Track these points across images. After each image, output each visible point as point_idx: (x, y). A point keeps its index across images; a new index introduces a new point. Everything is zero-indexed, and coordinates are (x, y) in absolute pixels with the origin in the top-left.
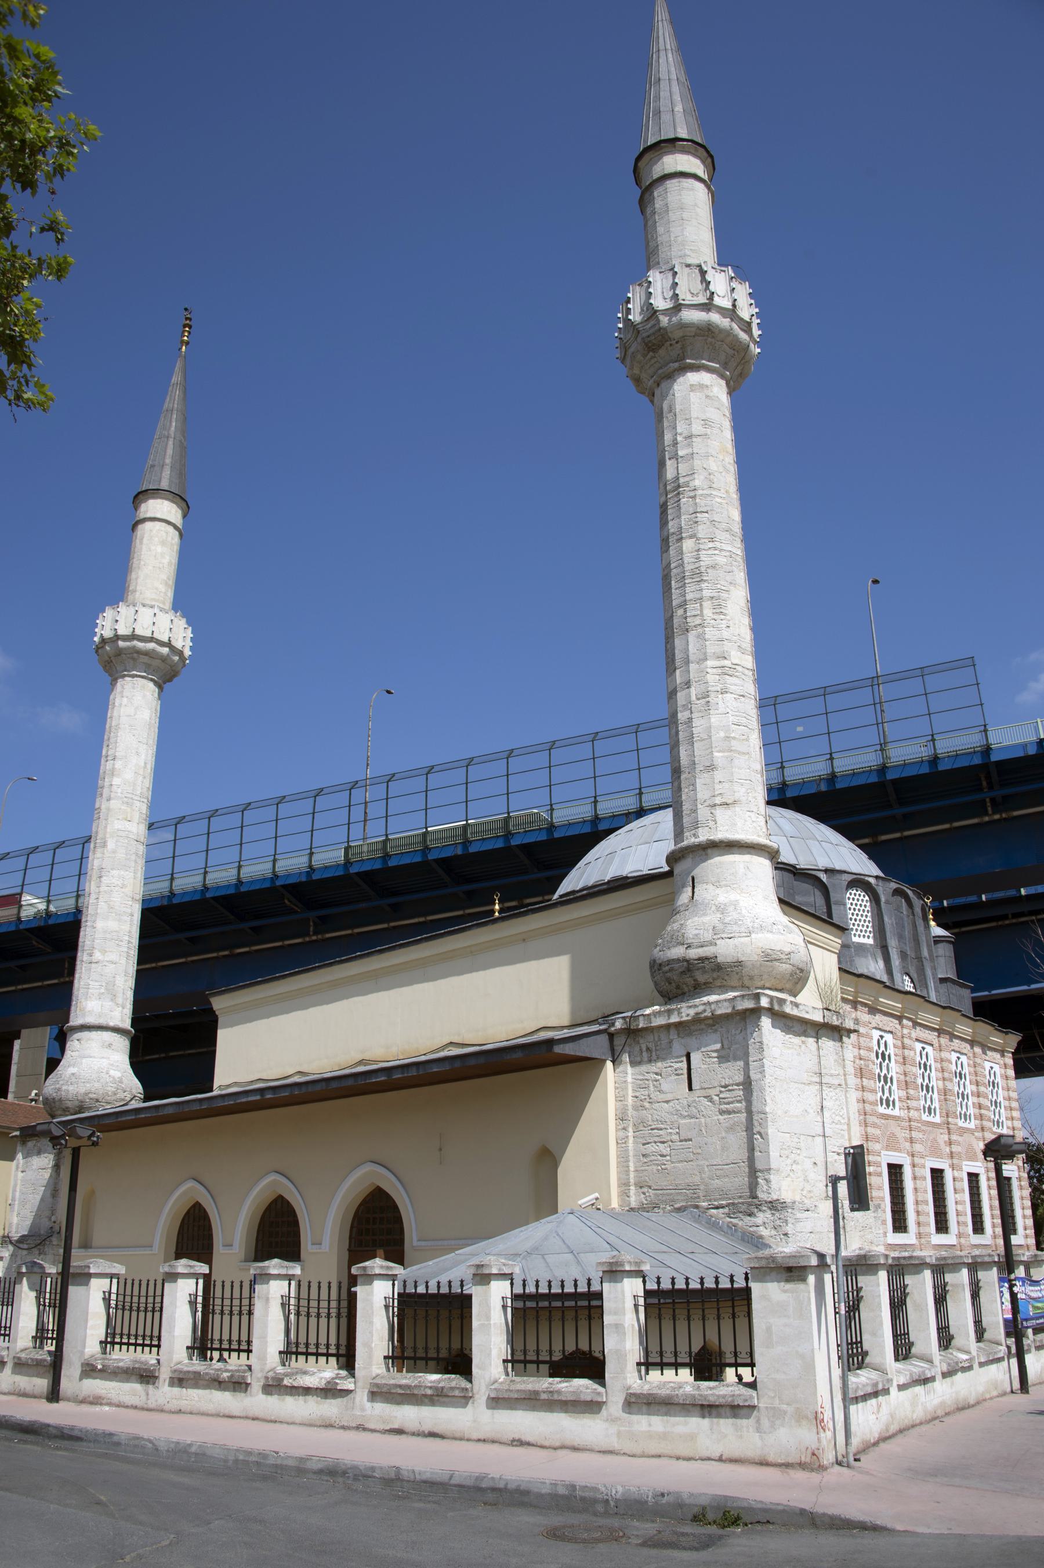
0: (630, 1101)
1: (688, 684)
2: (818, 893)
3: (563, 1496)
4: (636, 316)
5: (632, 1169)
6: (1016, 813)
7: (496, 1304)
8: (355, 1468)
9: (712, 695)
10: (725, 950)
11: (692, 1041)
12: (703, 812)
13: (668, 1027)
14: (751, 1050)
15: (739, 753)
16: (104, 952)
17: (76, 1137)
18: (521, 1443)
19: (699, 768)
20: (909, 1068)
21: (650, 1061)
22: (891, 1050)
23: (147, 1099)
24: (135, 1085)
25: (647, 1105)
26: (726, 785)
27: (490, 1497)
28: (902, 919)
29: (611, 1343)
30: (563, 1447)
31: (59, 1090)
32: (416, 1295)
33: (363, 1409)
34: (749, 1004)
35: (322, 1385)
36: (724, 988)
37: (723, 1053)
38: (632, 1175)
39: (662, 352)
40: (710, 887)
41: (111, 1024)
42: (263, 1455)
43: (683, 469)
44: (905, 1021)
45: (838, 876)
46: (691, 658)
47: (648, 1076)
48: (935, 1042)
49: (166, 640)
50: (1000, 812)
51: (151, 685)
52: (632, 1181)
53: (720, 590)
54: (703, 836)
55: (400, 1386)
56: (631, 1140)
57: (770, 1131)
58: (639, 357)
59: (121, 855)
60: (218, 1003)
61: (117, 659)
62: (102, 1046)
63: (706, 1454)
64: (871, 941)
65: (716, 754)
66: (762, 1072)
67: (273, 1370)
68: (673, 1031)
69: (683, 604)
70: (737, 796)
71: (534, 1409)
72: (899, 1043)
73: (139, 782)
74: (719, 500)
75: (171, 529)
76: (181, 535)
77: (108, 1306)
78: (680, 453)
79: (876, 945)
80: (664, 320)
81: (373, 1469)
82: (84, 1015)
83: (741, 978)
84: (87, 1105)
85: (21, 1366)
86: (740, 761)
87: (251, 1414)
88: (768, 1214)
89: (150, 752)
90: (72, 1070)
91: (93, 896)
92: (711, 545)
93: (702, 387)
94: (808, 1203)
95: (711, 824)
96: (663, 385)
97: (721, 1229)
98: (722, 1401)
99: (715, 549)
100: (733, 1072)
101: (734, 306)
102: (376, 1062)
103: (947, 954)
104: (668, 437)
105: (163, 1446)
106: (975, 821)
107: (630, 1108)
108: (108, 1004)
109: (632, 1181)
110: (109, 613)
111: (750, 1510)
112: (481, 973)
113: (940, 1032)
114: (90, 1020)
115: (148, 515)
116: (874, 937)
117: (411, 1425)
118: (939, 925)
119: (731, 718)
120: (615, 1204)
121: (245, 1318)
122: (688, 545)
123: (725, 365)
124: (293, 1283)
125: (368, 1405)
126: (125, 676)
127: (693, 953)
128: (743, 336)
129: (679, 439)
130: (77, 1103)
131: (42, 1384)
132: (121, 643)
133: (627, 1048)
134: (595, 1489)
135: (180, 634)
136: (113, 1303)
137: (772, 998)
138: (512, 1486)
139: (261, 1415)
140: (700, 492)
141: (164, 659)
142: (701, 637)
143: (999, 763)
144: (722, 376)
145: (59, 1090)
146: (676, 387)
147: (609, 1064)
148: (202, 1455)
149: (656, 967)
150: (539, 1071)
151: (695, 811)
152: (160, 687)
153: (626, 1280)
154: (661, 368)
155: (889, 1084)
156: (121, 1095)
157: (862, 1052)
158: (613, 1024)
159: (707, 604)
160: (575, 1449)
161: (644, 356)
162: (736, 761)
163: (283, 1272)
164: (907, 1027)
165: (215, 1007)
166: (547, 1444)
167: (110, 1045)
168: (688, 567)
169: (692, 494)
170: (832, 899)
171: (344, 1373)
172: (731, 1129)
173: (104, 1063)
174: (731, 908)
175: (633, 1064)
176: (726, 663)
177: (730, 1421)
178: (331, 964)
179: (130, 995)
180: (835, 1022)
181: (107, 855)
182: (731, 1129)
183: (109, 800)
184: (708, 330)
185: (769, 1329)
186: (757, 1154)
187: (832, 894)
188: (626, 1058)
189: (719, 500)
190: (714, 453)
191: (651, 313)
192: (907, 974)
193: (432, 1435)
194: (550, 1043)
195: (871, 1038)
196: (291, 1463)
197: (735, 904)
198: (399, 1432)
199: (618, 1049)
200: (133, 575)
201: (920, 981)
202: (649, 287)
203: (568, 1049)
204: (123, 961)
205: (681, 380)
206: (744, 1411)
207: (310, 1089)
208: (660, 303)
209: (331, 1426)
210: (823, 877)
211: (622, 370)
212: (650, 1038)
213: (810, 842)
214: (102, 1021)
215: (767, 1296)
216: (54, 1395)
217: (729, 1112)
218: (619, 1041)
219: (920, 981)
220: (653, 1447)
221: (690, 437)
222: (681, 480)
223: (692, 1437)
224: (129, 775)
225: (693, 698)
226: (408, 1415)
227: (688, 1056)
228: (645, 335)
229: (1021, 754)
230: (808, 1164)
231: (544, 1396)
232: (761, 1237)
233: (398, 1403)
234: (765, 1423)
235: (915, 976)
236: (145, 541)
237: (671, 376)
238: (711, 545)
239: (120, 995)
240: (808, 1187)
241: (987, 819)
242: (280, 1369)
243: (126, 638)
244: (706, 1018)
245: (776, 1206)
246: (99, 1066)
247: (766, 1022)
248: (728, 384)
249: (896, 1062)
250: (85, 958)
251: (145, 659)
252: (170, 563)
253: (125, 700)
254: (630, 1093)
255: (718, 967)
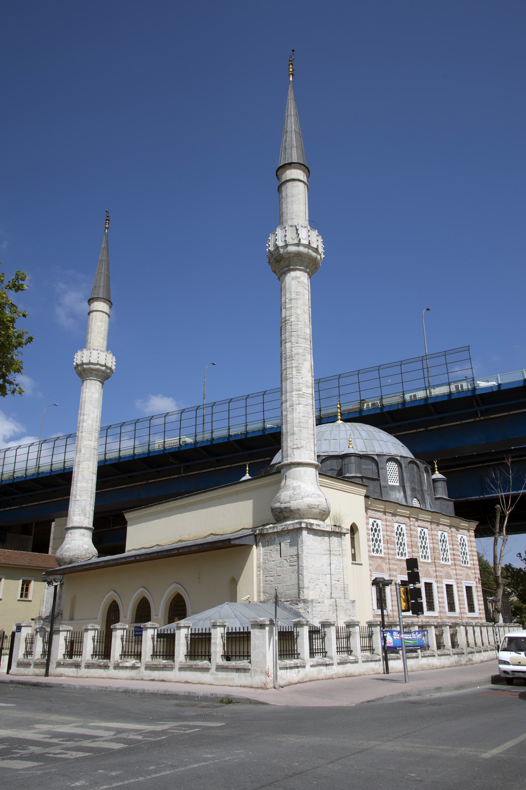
0: (262, 560)
1: (286, 401)
2: (374, 464)
3: (187, 696)
4: (272, 248)
5: (262, 586)
6: (491, 416)
7: (219, 636)
8: (132, 690)
9: (295, 405)
10: (294, 505)
11: (281, 539)
12: (290, 451)
13: (274, 533)
14: (299, 543)
15: (304, 428)
16: (81, 496)
17: (68, 573)
18: (187, 682)
19: (289, 434)
20: (413, 539)
21: (268, 545)
22: (404, 531)
23: (99, 556)
24: (95, 551)
25: (267, 562)
26: (298, 441)
27: (168, 697)
28: (414, 474)
29: (213, 649)
30: (199, 683)
31: (62, 554)
32: (167, 634)
33: (143, 673)
34: (298, 526)
35: (131, 665)
36: (294, 519)
37: (291, 543)
38: (262, 589)
39: (282, 263)
40: (291, 480)
41: (84, 526)
42: (107, 688)
43: (288, 313)
44: (411, 519)
45: (382, 457)
46: (288, 391)
47: (267, 551)
48: (429, 527)
49: (104, 364)
50: (484, 416)
51: (98, 383)
52: (262, 591)
53: (299, 363)
54: (289, 460)
55: (154, 665)
56: (261, 575)
57: (304, 573)
58: (274, 264)
59: (87, 455)
60: (128, 516)
61: (84, 372)
62: (80, 535)
63: (237, 684)
64: (398, 484)
65: (295, 429)
66: (302, 551)
67: (117, 661)
68: (276, 534)
69: (286, 369)
70: (302, 445)
71: (191, 671)
72: (409, 528)
73: (94, 424)
74: (300, 326)
75: (104, 315)
76: (109, 316)
77: (123, 641)
78: (287, 307)
79: (400, 486)
80: (282, 251)
81: (137, 690)
82: (73, 523)
83: (300, 515)
84: (74, 560)
85: (36, 665)
86: (305, 431)
87: (109, 677)
88: (302, 604)
89: (99, 411)
90: (67, 546)
91: (76, 473)
92: (297, 345)
93: (297, 278)
94: (320, 600)
95: (292, 455)
96: (282, 276)
97: (287, 609)
98: (241, 667)
99: (298, 346)
100: (293, 551)
101: (309, 243)
102: (185, 541)
103: (443, 486)
104: (283, 299)
105: (77, 687)
106: (472, 420)
107: (261, 563)
108: (83, 518)
109: (262, 591)
110: (79, 353)
111: (235, 698)
112: (222, 506)
113: (431, 522)
114: (75, 524)
115: (95, 309)
116: (400, 483)
117: (156, 678)
118: (440, 473)
119: (301, 414)
120: (255, 599)
121: (282, 649)
122: (288, 345)
123: (307, 267)
124: (189, 629)
125: (145, 671)
126: (87, 380)
127: (283, 506)
128: (314, 254)
129: (287, 300)
130: (69, 560)
131: (43, 671)
132: (85, 366)
133: (261, 541)
134: (195, 693)
135: (108, 360)
136: (125, 640)
137: (307, 524)
138: (174, 693)
139: (112, 677)
140: (294, 323)
141: (103, 372)
142: (291, 382)
143: (480, 395)
144: (306, 272)
145: (62, 554)
146: (287, 278)
147: (254, 547)
148: (89, 689)
149: (273, 510)
150: (226, 551)
151: (287, 450)
152: (102, 383)
153: (218, 628)
154: (282, 269)
155: (403, 546)
156: (88, 555)
157: (388, 533)
158: (256, 532)
159: (294, 369)
160: (202, 684)
161: (276, 264)
162: (302, 431)
163: (122, 627)
164: (412, 521)
165: (126, 518)
166: (194, 682)
167: (83, 535)
168: (288, 354)
169: (290, 324)
170: (379, 467)
171: (138, 661)
172: (293, 572)
173: (81, 542)
174: (297, 488)
175: (263, 546)
176: (300, 393)
177: (243, 674)
178: (169, 501)
179: (92, 513)
180: (337, 530)
181: (81, 455)
182: (293, 572)
183: (82, 432)
184: (299, 254)
185: (255, 644)
186: (300, 582)
187: (379, 465)
188: (260, 544)
189: (300, 326)
190: (300, 306)
191: (277, 248)
192: (416, 498)
193: (163, 681)
194: (229, 540)
195: (393, 527)
196: (114, 690)
197: (299, 486)
198: (153, 680)
199: (258, 540)
200: (89, 336)
201: (422, 501)
202: (276, 236)
203: (237, 542)
204: (89, 499)
205: (288, 275)
206: (247, 671)
207: (152, 555)
208: (280, 243)
209: (133, 679)
210: (376, 458)
211: (269, 267)
212: (268, 537)
213: (374, 441)
214: (80, 525)
215: (255, 633)
216: (47, 674)
217: (292, 566)
218: (258, 538)
219: (422, 500)
220: (223, 683)
221: (291, 300)
222: (287, 318)
223: (233, 679)
224: (90, 422)
225: (288, 406)
226: (156, 674)
227: (280, 544)
228: (275, 256)
229: (490, 391)
230: (323, 585)
231: (194, 667)
232: (300, 613)
233: (153, 670)
234: (253, 674)
235: (420, 498)
236: (93, 320)
237: (285, 273)
238: (297, 345)
239: (88, 513)
240: (322, 594)
241: (478, 419)
242: (120, 661)
243: (86, 364)
244: (286, 530)
245: (305, 601)
246: (78, 543)
247: (305, 533)
248: (309, 274)
249: (407, 536)
250: (73, 499)
251: (96, 372)
252: (105, 330)
253: (88, 390)
254: (262, 557)
255: (291, 511)
